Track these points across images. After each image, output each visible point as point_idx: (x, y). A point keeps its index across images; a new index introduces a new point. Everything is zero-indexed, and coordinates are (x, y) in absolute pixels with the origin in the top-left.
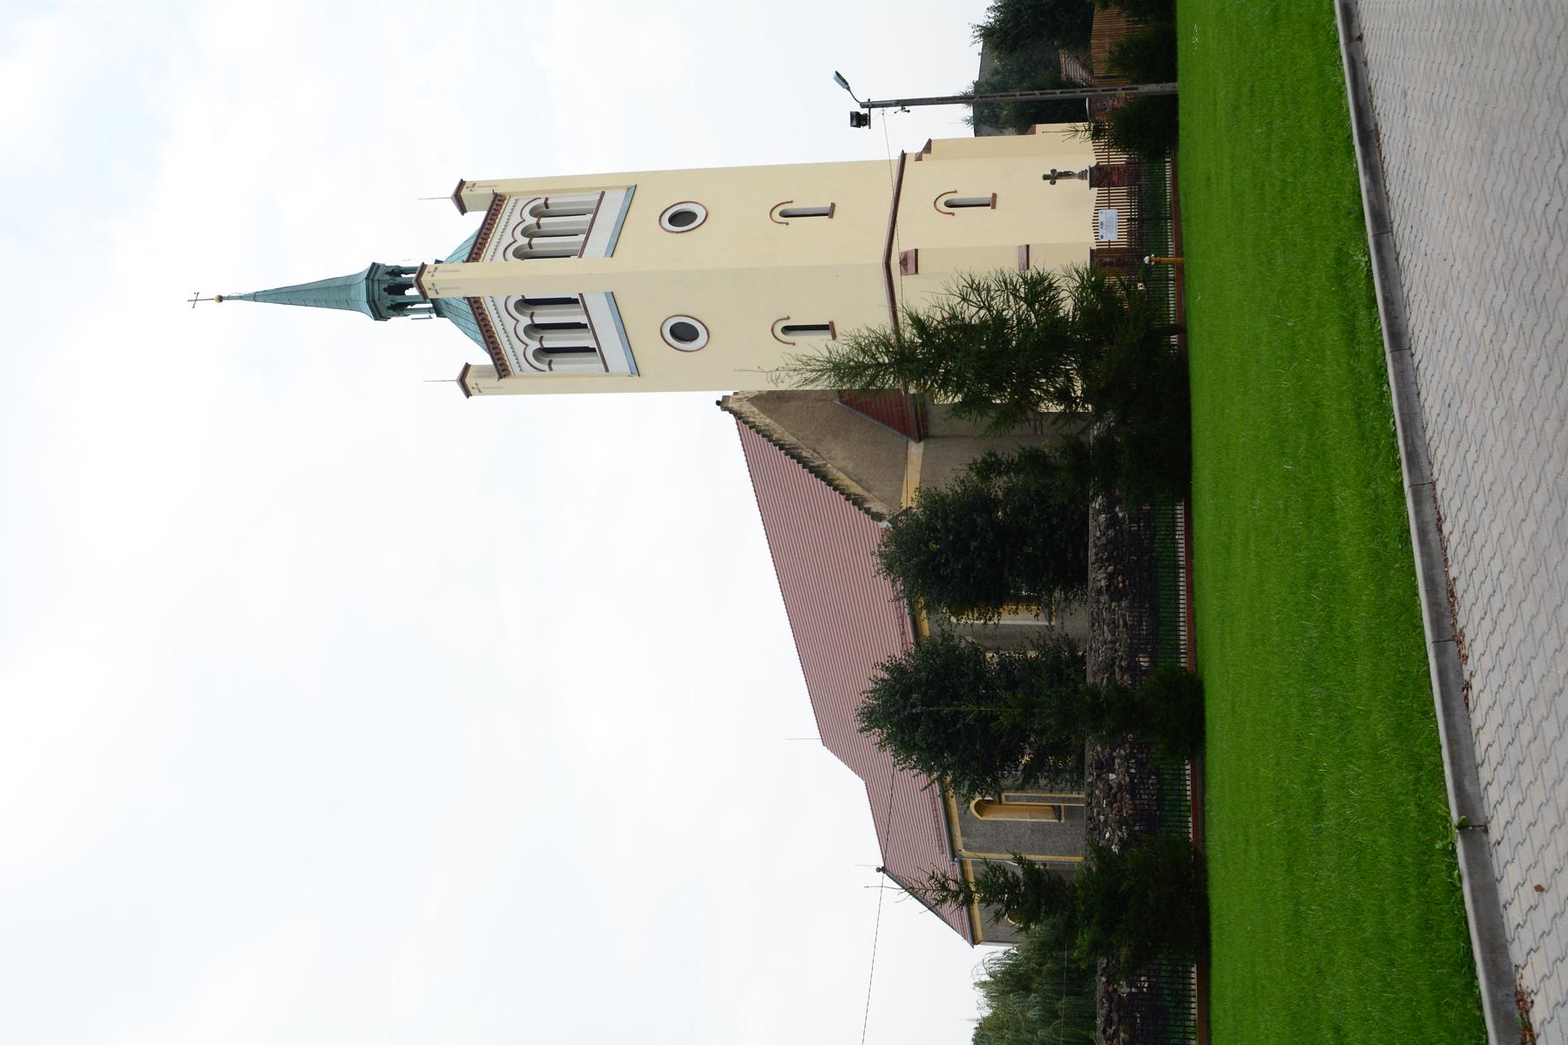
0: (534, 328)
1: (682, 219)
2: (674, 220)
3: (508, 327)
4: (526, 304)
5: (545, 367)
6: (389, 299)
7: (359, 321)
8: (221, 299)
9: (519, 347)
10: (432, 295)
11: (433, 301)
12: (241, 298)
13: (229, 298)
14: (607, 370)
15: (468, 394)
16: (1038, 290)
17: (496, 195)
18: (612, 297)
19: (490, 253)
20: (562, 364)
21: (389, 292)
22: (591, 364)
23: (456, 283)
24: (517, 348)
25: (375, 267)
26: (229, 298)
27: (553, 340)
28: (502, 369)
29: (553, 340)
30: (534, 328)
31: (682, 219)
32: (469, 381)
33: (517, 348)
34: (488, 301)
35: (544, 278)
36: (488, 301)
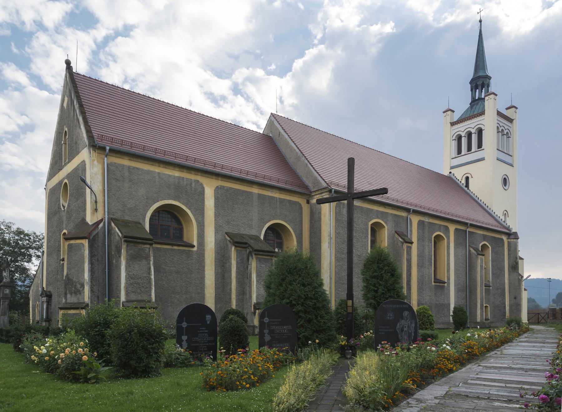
0: (469, 135)
1: (505, 181)
2: (505, 179)
3: (472, 125)
4: (480, 132)
5: (454, 138)
6: (480, 83)
7: (470, 73)
8: (480, 21)
9: (462, 129)
10: (486, 98)
11: (484, 99)
12: (481, 28)
13: (481, 25)
14: (351, 162)
15: (444, 112)
16: (365, 286)
17: (513, 120)
18: (483, 159)
19: (499, 119)
20: (454, 144)
21: (480, 82)
22: (454, 154)
23: (490, 105)
24: (462, 129)
25: (490, 78)
26: (481, 25)
27: (464, 141)
28: (452, 124)
29: (464, 141)
30: (469, 135)
31: (505, 181)
32: (449, 112)
33: (462, 129)
34: (483, 118)
35: (490, 137)
36: (483, 118)
